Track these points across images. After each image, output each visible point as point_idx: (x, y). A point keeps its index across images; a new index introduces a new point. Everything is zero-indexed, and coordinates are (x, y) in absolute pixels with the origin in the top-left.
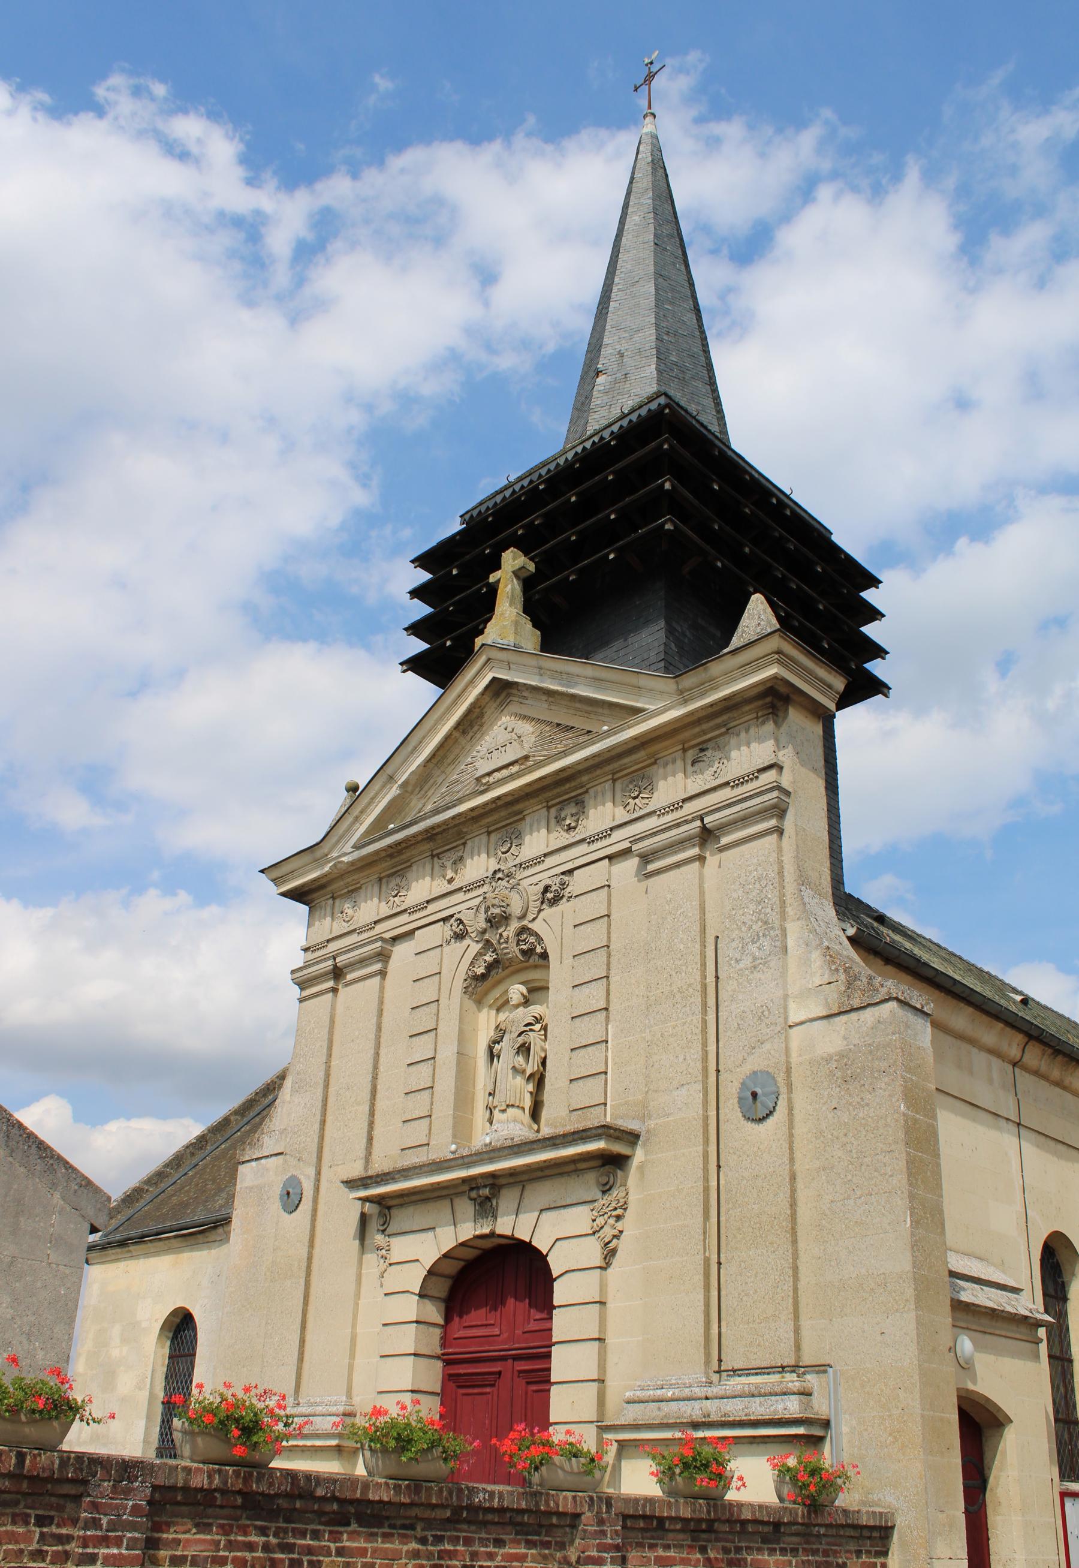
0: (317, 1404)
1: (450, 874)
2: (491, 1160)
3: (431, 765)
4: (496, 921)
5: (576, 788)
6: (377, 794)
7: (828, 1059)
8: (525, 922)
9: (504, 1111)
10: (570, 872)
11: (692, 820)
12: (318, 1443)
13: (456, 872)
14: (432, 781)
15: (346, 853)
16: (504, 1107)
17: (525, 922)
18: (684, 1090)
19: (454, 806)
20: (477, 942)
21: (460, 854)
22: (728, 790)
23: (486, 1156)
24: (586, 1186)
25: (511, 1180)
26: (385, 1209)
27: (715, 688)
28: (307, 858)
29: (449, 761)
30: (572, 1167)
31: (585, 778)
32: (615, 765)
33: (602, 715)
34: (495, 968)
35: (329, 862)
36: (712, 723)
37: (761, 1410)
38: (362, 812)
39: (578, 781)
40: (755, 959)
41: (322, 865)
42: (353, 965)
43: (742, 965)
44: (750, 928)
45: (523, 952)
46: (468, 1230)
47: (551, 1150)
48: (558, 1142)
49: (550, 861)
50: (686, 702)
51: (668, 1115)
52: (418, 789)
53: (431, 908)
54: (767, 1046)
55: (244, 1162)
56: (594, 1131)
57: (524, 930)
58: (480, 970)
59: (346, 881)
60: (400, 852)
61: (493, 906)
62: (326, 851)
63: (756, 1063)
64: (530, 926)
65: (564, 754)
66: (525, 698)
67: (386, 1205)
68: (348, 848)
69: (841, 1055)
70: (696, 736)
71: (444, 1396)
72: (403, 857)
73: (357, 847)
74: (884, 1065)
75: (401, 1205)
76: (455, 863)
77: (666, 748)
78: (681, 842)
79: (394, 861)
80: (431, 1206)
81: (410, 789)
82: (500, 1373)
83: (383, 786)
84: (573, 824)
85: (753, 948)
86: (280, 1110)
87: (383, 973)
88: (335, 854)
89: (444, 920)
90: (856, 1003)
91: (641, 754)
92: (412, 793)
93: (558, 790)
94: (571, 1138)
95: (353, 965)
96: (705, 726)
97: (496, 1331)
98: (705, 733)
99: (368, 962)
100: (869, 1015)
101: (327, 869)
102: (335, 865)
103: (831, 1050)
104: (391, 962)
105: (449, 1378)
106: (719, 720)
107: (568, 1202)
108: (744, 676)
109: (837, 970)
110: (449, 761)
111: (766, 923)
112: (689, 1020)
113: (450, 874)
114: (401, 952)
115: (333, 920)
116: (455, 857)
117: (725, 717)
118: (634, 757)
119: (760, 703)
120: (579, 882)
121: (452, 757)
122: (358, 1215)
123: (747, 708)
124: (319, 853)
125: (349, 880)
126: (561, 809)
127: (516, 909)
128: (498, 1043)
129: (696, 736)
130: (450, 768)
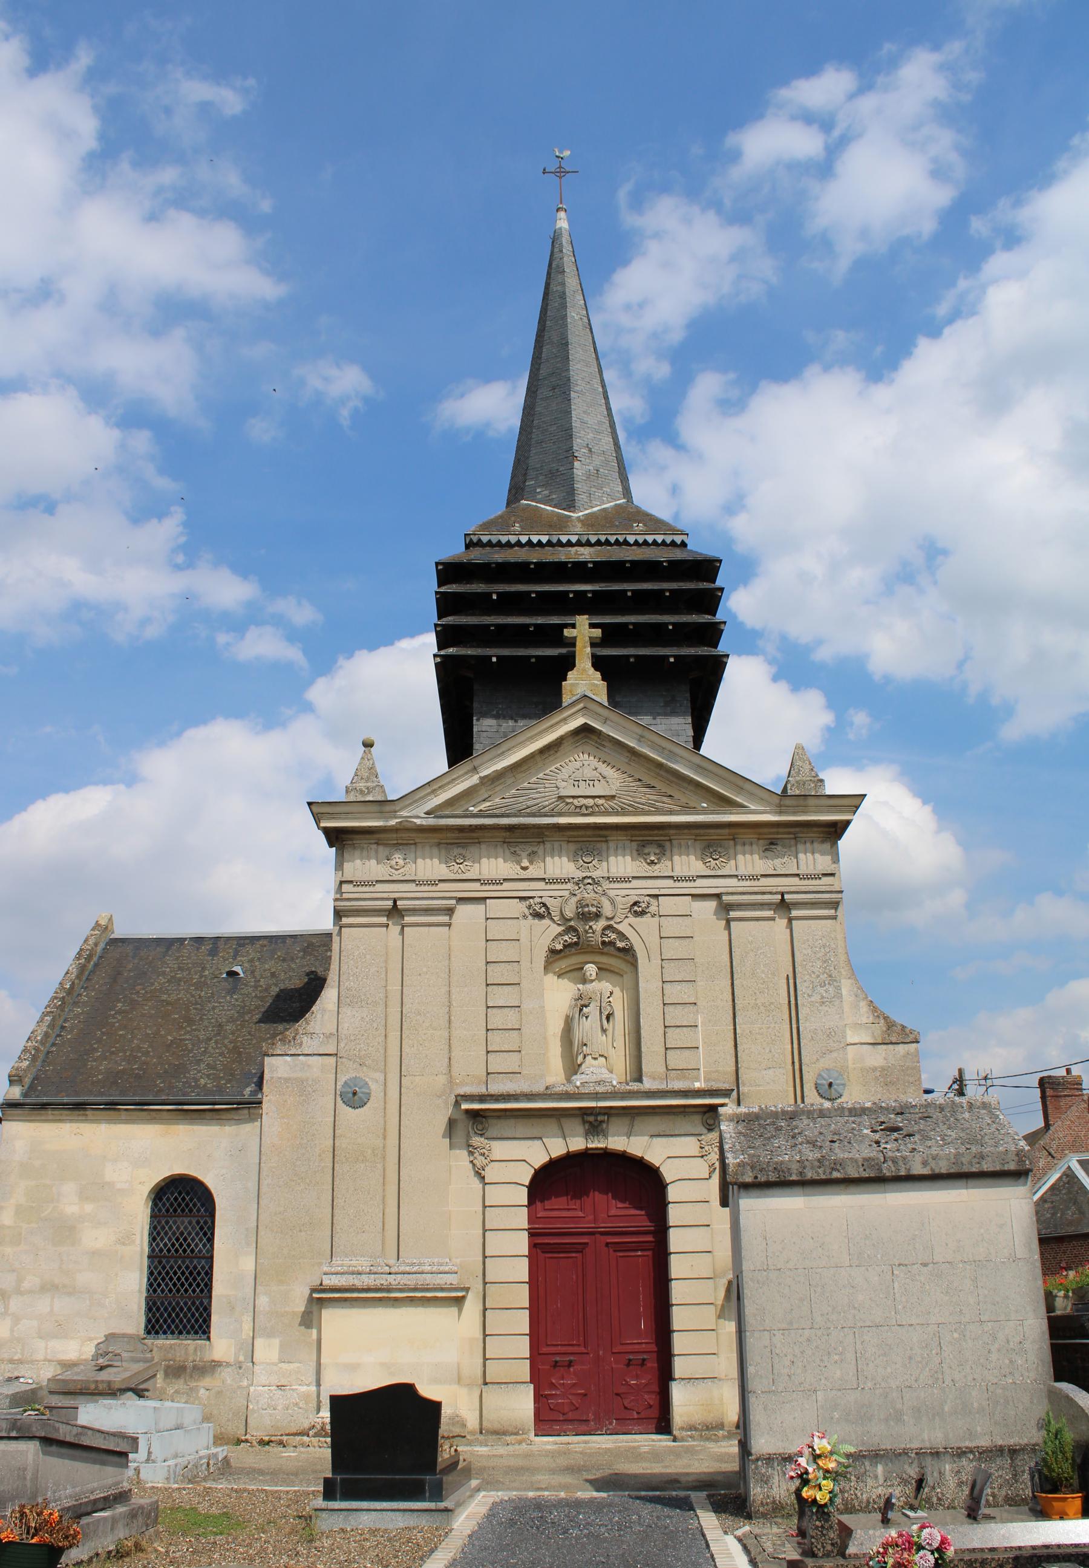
0: (413, 1264)
1: (525, 863)
2: (622, 1098)
4: (586, 916)
5: (661, 835)
6: (458, 777)
7: (874, 1069)
8: (612, 922)
9: (595, 1059)
10: (656, 896)
11: (776, 893)
12: (355, 1295)
13: (531, 862)
15: (418, 815)
17: (612, 922)
18: (771, 1072)
22: (797, 879)
24: (695, 1124)
26: (477, 1119)
27: (805, 812)
28: (374, 808)
31: (672, 832)
32: (702, 831)
33: (686, 789)
37: (438, 1281)
40: (823, 997)
41: (387, 819)
43: (813, 999)
44: (818, 976)
45: (603, 943)
46: (578, 1144)
49: (635, 883)
50: (780, 813)
53: (506, 886)
54: (835, 1055)
55: (273, 1055)
58: (559, 947)
59: (399, 835)
63: (826, 1063)
64: (615, 926)
65: (671, 812)
66: (603, 746)
67: (475, 1116)
68: (421, 810)
69: (883, 1069)
70: (770, 833)
71: (532, 1257)
74: (911, 1079)
76: (529, 855)
77: (744, 834)
78: (762, 904)
79: (461, 835)
80: (543, 1120)
82: (587, 1244)
83: (466, 773)
85: (822, 990)
86: (319, 1016)
88: (404, 813)
90: (894, 1040)
91: (726, 831)
96: (781, 830)
97: (581, 1214)
98: (778, 833)
100: (901, 1048)
103: (876, 1065)
105: (533, 1246)
108: (829, 812)
109: (878, 1017)
111: (830, 976)
112: (772, 1025)
113: (525, 863)
117: (797, 829)
120: (667, 905)
122: (447, 1119)
124: (388, 808)
127: (607, 910)
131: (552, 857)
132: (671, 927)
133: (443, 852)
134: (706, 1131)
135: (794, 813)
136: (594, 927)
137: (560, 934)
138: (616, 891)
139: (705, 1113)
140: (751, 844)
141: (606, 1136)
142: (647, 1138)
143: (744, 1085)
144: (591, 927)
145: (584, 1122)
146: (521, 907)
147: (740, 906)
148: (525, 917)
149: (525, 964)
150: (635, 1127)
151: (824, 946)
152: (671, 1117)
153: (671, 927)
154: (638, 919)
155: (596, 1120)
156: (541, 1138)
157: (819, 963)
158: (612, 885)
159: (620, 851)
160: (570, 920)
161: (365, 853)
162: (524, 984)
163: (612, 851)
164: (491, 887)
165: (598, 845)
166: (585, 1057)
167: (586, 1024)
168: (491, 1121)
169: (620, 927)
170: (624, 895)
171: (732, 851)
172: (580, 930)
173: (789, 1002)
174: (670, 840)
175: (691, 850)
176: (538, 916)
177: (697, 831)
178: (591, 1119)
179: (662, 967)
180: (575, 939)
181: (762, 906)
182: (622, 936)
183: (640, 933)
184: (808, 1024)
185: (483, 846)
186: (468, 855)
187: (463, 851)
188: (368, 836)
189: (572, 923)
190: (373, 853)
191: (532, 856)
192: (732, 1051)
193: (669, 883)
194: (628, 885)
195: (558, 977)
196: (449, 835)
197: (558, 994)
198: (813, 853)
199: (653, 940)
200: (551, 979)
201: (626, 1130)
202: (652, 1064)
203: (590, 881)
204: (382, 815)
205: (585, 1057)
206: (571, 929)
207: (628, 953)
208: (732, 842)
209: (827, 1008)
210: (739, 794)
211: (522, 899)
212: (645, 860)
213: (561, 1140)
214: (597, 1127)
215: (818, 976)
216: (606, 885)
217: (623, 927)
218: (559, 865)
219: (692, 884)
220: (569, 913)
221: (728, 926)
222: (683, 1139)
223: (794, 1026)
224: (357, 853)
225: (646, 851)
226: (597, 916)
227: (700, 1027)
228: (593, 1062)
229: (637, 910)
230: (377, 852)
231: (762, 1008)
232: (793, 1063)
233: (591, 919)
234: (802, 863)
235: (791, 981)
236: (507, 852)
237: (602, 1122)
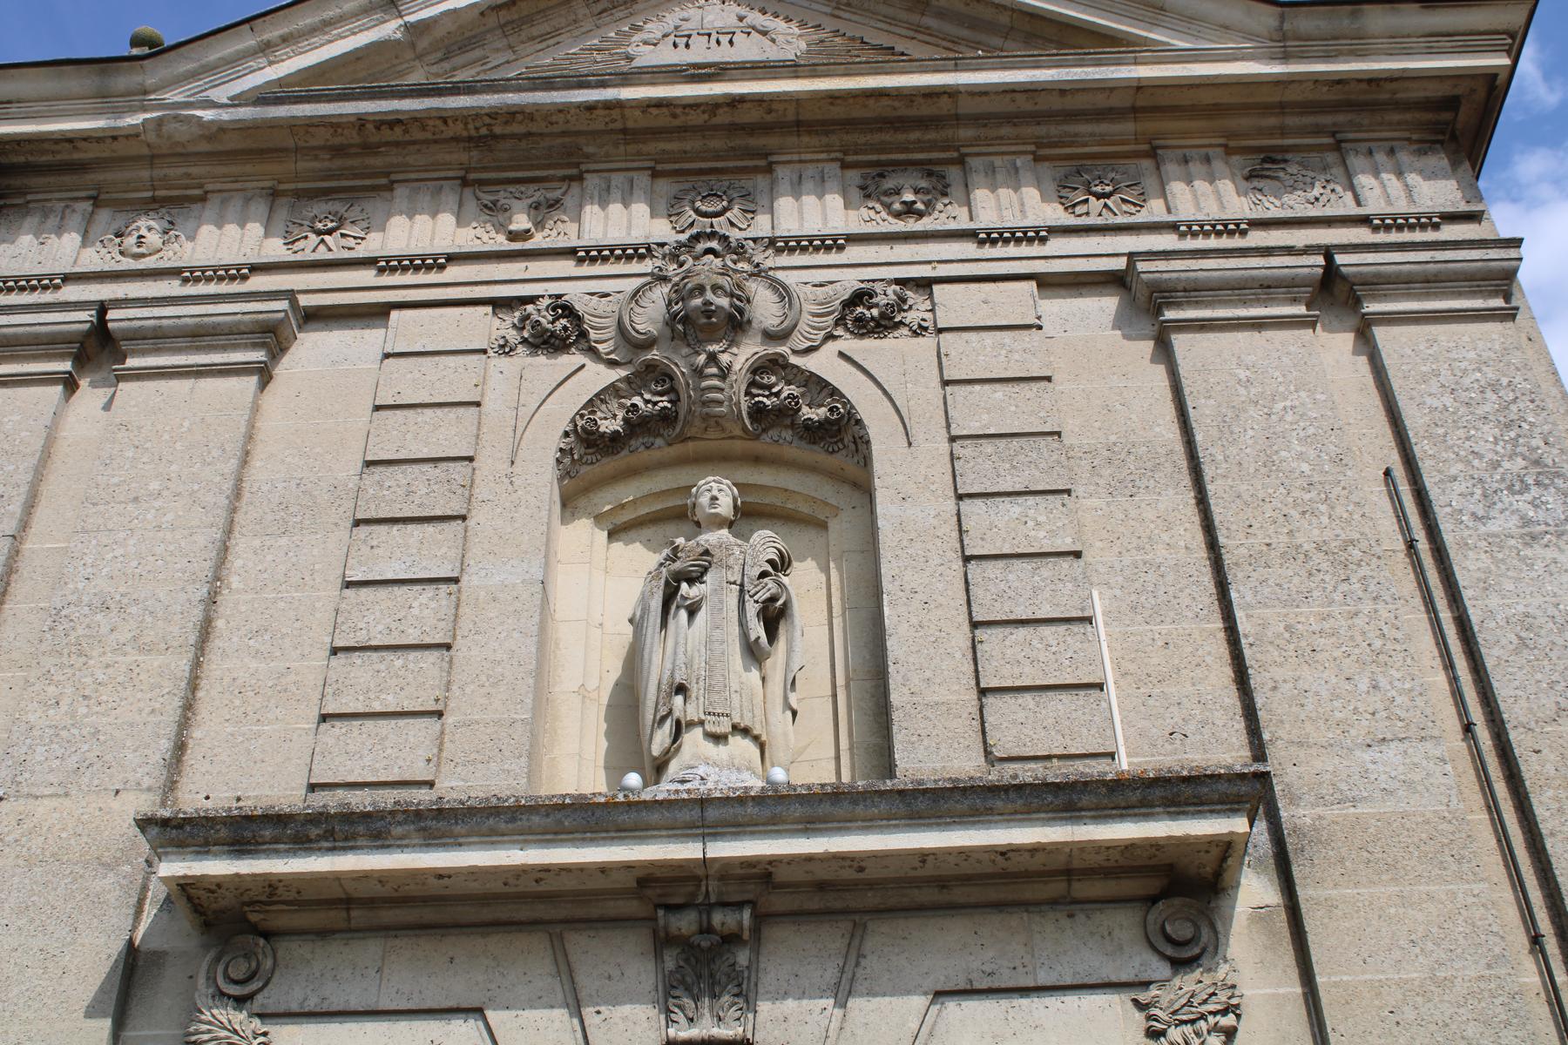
1: (521, 222)
2: (809, 826)
3: (492, 21)
5: (933, 146)
8: (783, 349)
9: (718, 738)
10: (925, 285)
14: (478, 53)
16: (724, 727)
17: (783, 349)
18: (1392, 752)
19: (603, 85)
20: (613, 364)
21: (557, 194)
23: (797, 811)
25: (815, 903)
29: (535, 31)
30: (1056, 888)
31: (965, 133)
32: (1054, 130)
34: (649, 432)
35: (145, 109)
36: (1308, 120)
38: (285, 40)
39: (949, 133)
40: (1526, 522)
41: (118, 112)
42: (157, 338)
43: (1493, 527)
45: (758, 412)
47: (1047, 822)
48: (1086, 800)
49: (854, 253)
50: (1285, 57)
51: (1354, 802)
52: (439, 55)
53: (453, 273)
56: (1222, 787)
57: (774, 364)
58: (609, 426)
59: (158, 173)
60: (368, 148)
61: (716, 288)
62: (150, 81)
64: (794, 360)
70: (1261, 132)
72: (377, 162)
73: (237, 101)
75: (323, 934)
77: (1185, 134)
80: (496, 943)
81: (423, 44)
84: (920, 206)
85: (1521, 503)
87: (264, 374)
89: (498, 304)
91: (1127, 127)
92: (419, 57)
93: (887, 137)
94: (1135, 797)
95: (157, 338)
96: (1292, 121)
98: (1283, 131)
99: (222, 340)
101: (136, 119)
102: (160, 122)
104: (286, 360)
106: (1326, 120)
107: (1044, 978)
108: (1430, 52)
110: (535, 31)
112: (1367, 607)
113: (521, 222)
114: (314, 350)
115: (84, 244)
116: (538, 196)
117: (1341, 118)
118: (1104, 128)
119: (1429, 116)
120: (953, 303)
121: (545, 28)
122: (117, 946)
123: (1396, 117)
125: (171, 172)
126: (882, 176)
128: (691, 582)
129: (1261, 132)
130: (530, 48)
131: (603, 204)
132: (968, 355)
133: (282, 214)
134: (1163, 970)
135: (1327, 57)
136: (725, 358)
137: (612, 390)
138: (799, 273)
139: (1153, 900)
140: (1207, 160)
141: (746, 997)
142: (919, 1002)
143: (1294, 800)
144: (712, 358)
145: (663, 942)
146: (502, 326)
147: (1194, 291)
148: (505, 349)
149: (490, 464)
150: (871, 963)
151: (1494, 386)
152: (1015, 920)
153: (968, 355)
154: (870, 343)
155: (707, 930)
156: (478, 1011)
157: (1489, 431)
158: (785, 260)
159: (808, 185)
160: (650, 343)
161: (53, 221)
162: (478, 517)
163: (784, 185)
164: (410, 278)
165: (746, 182)
166: (677, 734)
167: (689, 635)
168: (291, 949)
169: (810, 363)
170: (818, 283)
171: (1150, 182)
172: (681, 369)
173: (1411, 545)
174: (961, 161)
175: (1026, 175)
176: (545, 342)
177: (1041, 130)
178: (685, 923)
179: (952, 457)
180: (664, 402)
181: (1266, 288)
182: (819, 386)
183: (879, 380)
184: (1494, 601)
185: (401, 192)
186: (355, 213)
187: (339, 207)
188: (67, 179)
189: (654, 354)
190: (76, 219)
191: (544, 210)
192: (1231, 698)
193: (968, 249)
194: (833, 258)
195: (613, 535)
196: (304, 165)
197: (601, 580)
198: (1400, 174)
199: (922, 396)
200: (583, 535)
201: (831, 974)
202: (927, 671)
203: (714, 244)
204: (104, 100)
205: (677, 734)
206: (653, 375)
207: (841, 434)
208: (1147, 164)
209: (1550, 554)
210: (1154, 24)
211: (498, 304)
212: (888, 206)
213: (560, 1015)
214: (712, 954)
215: (1496, 465)
216: (770, 260)
217: (823, 363)
218: (624, 219)
219: (1035, 249)
220: (650, 316)
221: (1164, 351)
222: (1072, 1000)
223: (1446, 615)
224: (31, 221)
225: (889, 184)
226: (736, 324)
227: (1100, 619)
228: (710, 748)
229: (866, 315)
230: (89, 220)
231: (1318, 558)
232: (1468, 728)
233: (711, 334)
234: (1365, 194)
235: (1405, 489)
236: (471, 206)
237: (731, 939)
